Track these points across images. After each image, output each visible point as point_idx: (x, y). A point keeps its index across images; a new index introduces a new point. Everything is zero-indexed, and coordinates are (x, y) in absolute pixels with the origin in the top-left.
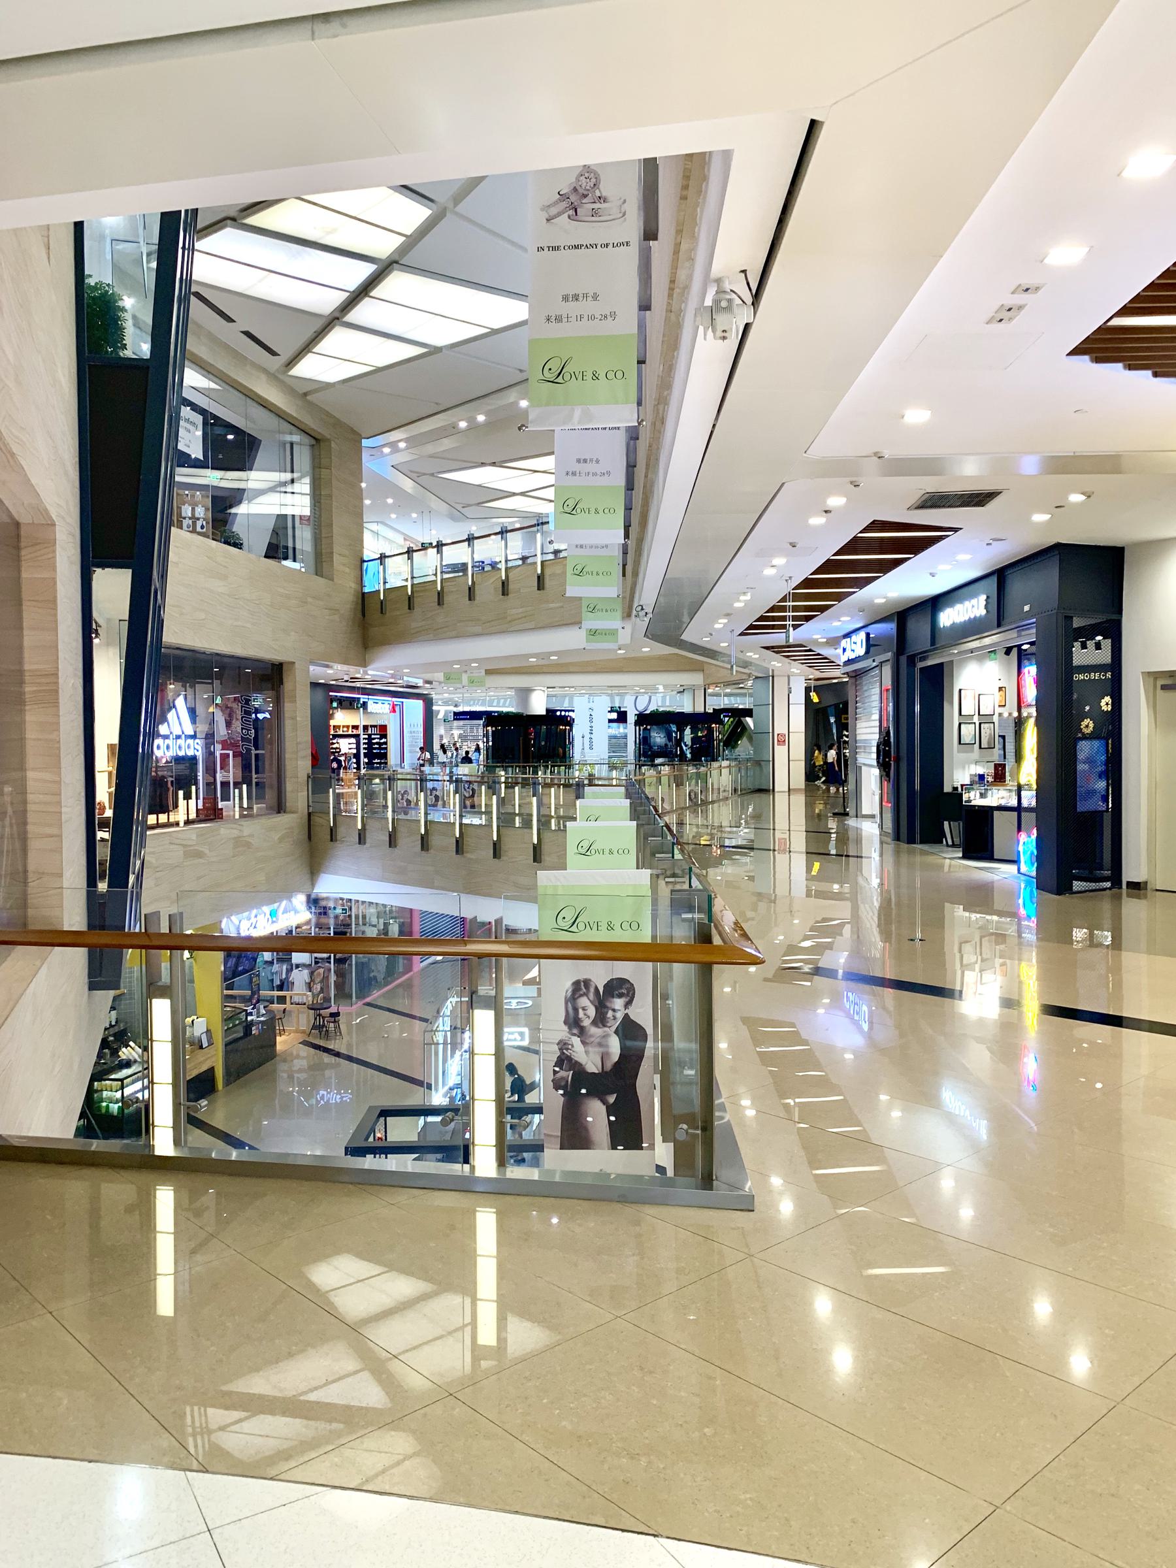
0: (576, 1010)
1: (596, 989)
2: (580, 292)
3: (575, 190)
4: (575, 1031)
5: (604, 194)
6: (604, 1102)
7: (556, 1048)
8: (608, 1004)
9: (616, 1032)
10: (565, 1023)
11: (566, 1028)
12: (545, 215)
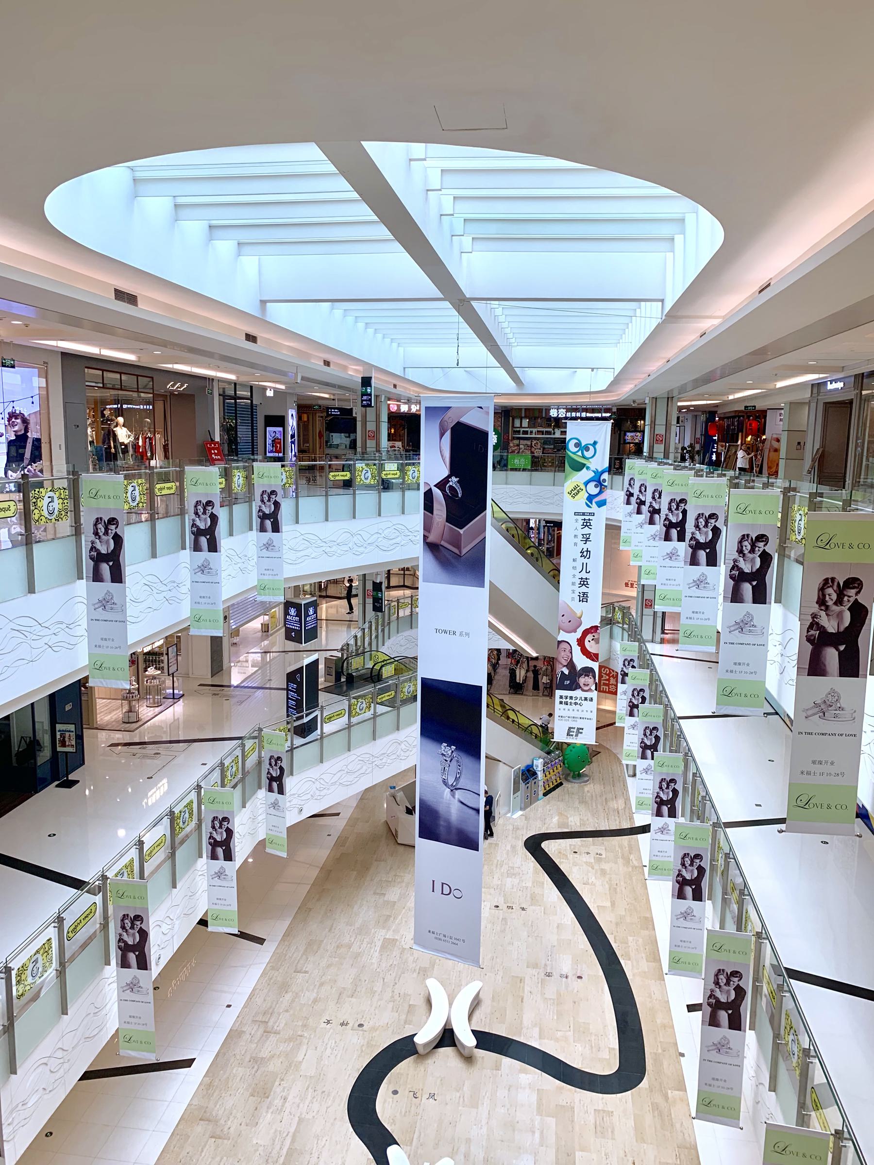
0: (824, 596)
2: (823, 760)
3: (825, 702)
5: (843, 706)
6: (837, 649)
8: (845, 593)
9: (848, 609)
11: (817, 606)
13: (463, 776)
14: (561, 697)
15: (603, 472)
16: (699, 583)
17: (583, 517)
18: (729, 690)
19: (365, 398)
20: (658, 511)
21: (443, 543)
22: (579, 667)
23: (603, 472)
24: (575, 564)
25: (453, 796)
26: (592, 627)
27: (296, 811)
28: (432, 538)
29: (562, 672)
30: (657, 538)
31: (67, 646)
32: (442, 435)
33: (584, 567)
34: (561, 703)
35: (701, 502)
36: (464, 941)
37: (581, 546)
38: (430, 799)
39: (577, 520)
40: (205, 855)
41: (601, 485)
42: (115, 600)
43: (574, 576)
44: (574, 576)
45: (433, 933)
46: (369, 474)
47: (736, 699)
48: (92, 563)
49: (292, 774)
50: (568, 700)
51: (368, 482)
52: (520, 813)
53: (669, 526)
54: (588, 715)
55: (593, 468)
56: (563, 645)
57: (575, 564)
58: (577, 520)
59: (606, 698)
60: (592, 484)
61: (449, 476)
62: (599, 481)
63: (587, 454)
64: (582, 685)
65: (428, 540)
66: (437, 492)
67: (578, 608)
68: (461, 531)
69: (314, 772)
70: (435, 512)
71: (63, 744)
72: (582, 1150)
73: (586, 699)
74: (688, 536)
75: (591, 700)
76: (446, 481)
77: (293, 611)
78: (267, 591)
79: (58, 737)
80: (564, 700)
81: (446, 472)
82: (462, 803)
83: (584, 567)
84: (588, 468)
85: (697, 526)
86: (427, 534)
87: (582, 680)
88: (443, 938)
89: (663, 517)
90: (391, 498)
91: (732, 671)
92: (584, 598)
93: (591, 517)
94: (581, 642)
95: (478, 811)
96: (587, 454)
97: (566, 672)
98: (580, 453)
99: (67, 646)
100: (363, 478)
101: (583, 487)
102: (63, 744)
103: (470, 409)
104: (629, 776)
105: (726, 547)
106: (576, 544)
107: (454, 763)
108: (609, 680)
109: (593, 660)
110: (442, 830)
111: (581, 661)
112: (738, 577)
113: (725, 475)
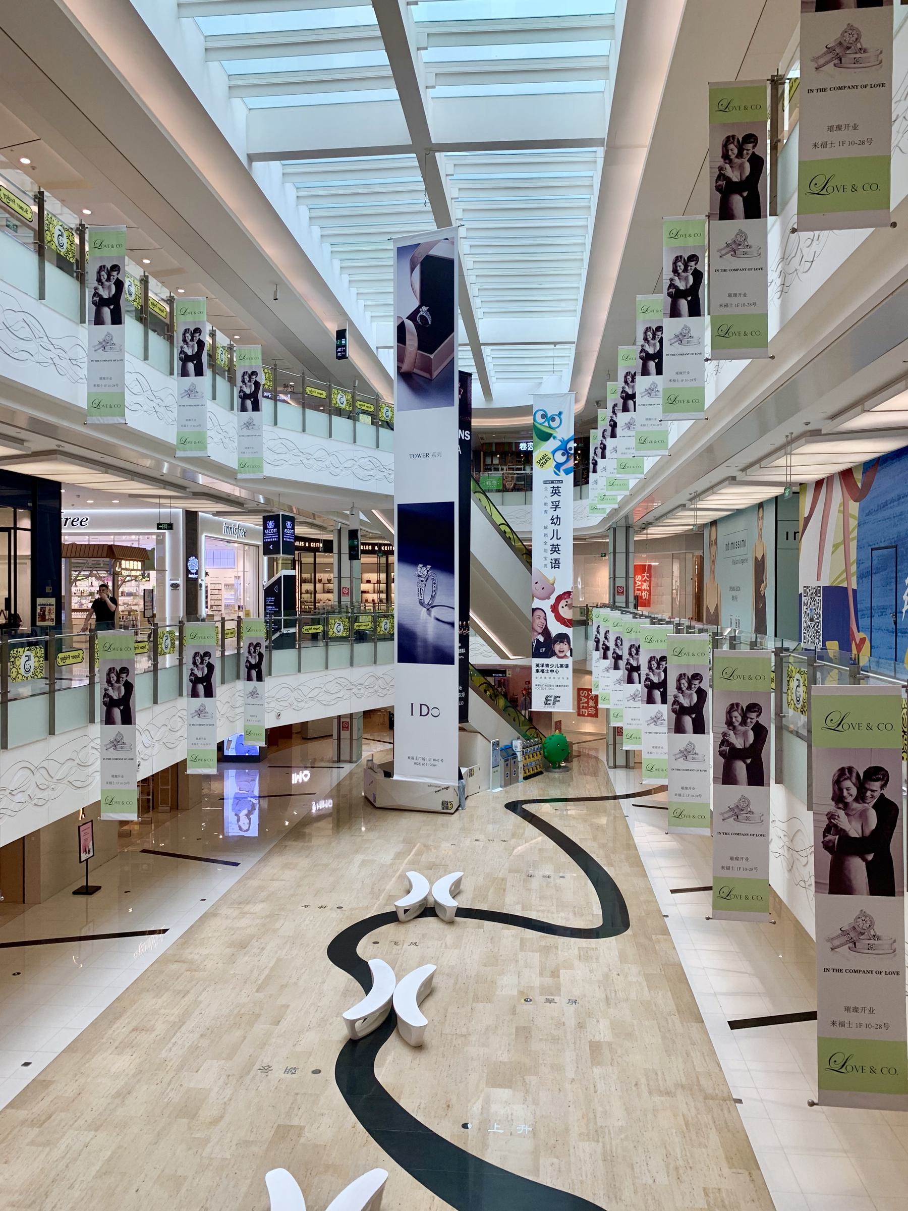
1: (858, 774)
4: (841, 806)
5: (864, 46)
6: (742, 196)
7: (825, 818)
8: (867, 786)
9: (874, 807)
10: (833, 799)
12: (829, 945)
13: (438, 593)
14: (537, 665)
15: (568, 441)
16: (687, 753)
17: (552, 485)
18: (673, 398)
19: (340, 349)
20: (637, 669)
21: (416, 371)
22: (554, 634)
23: (568, 441)
24: (546, 531)
25: (429, 614)
26: (565, 593)
27: (274, 715)
28: (405, 367)
29: (538, 640)
30: (637, 699)
31: (9, 813)
32: (412, 270)
33: (555, 534)
34: (537, 671)
35: (683, 660)
36: (442, 760)
37: (551, 513)
38: (408, 623)
39: (546, 489)
40: (185, 693)
41: (568, 453)
42: (114, 341)
43: (546, 543)
44: (546, 543)
45: (413, 758)
46: (341, 627)
47: (735, 895)
48: (95, 308)
49: (270, 674)
50: (544, 668)
51: (340, 634)
52: (500, 789)
53: (651, 687)
54: (565, 682)
55: (559, 437)
56: (538, 613)
57: (546, 531)
58: (546, 489)
59: (586, 722)
60: (559, 453)
61: (420, 307)
62: (566, 450)
63: (553, 424)
64: (557, 652)
65: (402, 370)
66: (409, 324)
67: (551, 574)
68: (432, 356)
69: (294, 680)
70: (407, 343)
71: (43, 619)
72: (565, 968)
73: (562, 666)
74: (670, 699)
75: (567, 666)
76: (417, 311)
77: (271, 524)
78: (247, 469)
79: (38, 611)
80: (540, 668)
81: (416, 303)
82: (438, 620)
83: (555, 534)
84: (554, 438)
85: (679, 688)
86: (400, 365)
87: (557, 647)
88: (422, 762)
89: (643, 678)
90: (363, 649)
91: (674, 381)
92: (556, 564)
93: (559, 485)
94: (554, 608)
95: (452, 624)
96: (553, 424)
97: (542, 639)
98: (546, 424)
99: (9, 813)
100: (335, 630)
101: (551, 456)
102: (43, 619)
103: (436, 242)
104: (610, 767)
105: (713, 712)
106: (546, 512)
107: (430, 581)
108: (587, 703)
109: (567, 626)
110: (420, 651)
111: (556, 628)
112: (729, 755)
113: (706, 631)
